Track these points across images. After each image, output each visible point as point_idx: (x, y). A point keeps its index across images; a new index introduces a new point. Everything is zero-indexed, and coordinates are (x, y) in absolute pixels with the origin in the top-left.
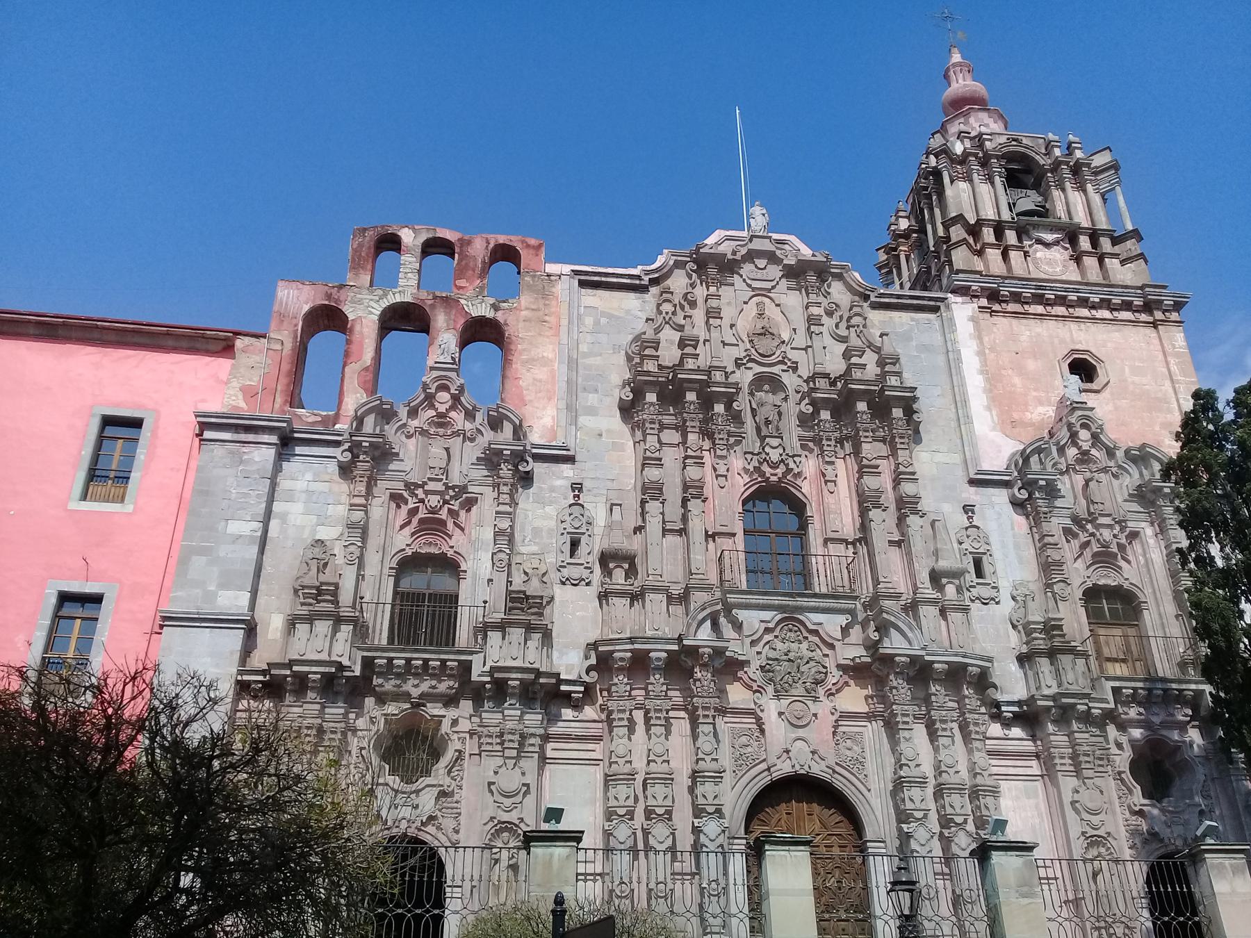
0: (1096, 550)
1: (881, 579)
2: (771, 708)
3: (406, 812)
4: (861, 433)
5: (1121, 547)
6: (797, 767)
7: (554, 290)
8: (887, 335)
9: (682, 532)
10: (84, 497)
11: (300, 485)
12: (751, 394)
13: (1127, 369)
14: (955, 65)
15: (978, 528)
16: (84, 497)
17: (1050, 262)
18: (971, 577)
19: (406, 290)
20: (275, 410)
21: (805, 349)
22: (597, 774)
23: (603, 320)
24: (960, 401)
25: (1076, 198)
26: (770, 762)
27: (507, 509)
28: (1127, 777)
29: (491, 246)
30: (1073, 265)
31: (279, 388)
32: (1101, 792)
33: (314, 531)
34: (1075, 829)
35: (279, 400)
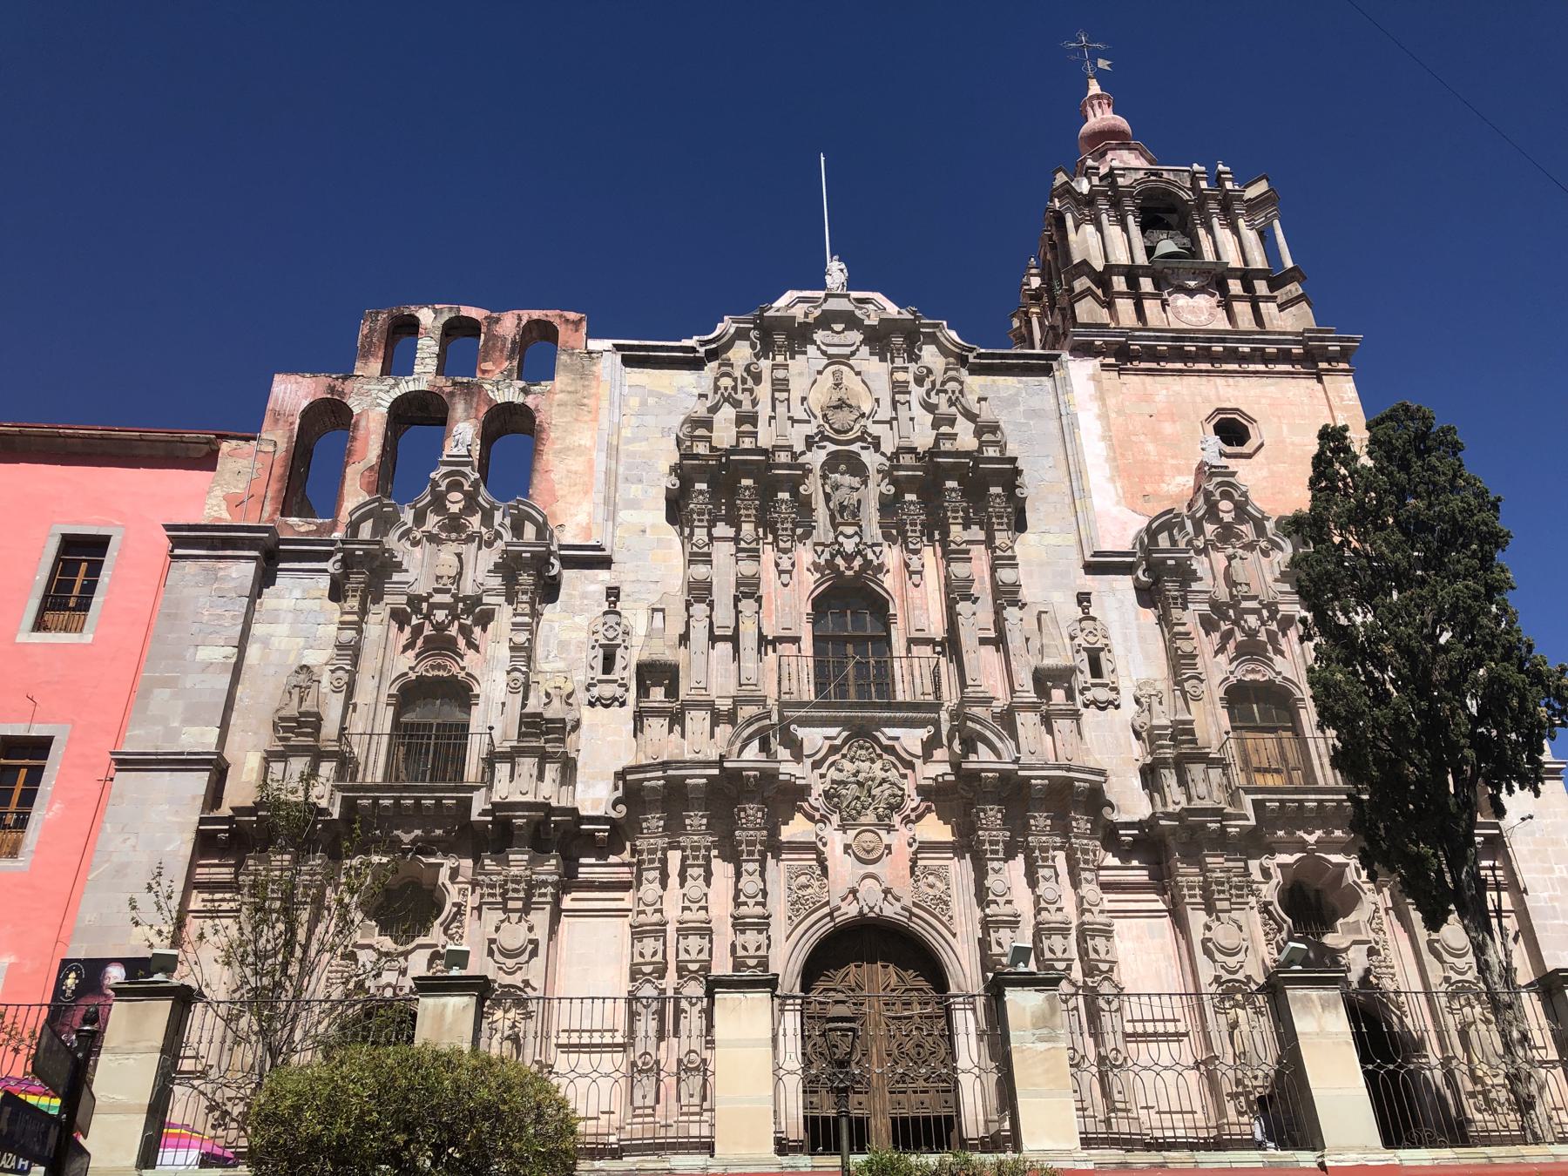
1: (969, 682)
2: (835, 841)
3: (389, 977)
4: (949, 514)
5: (1272, 637)
7: (594, 368)
8: (985, 399)
9: (734, 639)
10: (40, 625)
11: (287, 603)
12: (824, 477)
13: (1285, 428)
14: (1092, 97)
15: (1094, 619)
16: (40, 625)
17: (1193, 311)
18: (1085, 677)
19: (424, 375)
20: (263, 519)
21: (889, 422)
22: (622, 927)
23: (651, 401)
24: (1074, 472)
25: (1224, 235)
27: (527, 619)
28: (1277, 908)
29: (524, 322)
30: (1221, 314)
31: (269, 495)
32: (1240, 928)
33: (301, 655)
34: (1207, 971)
35: (268, 509)
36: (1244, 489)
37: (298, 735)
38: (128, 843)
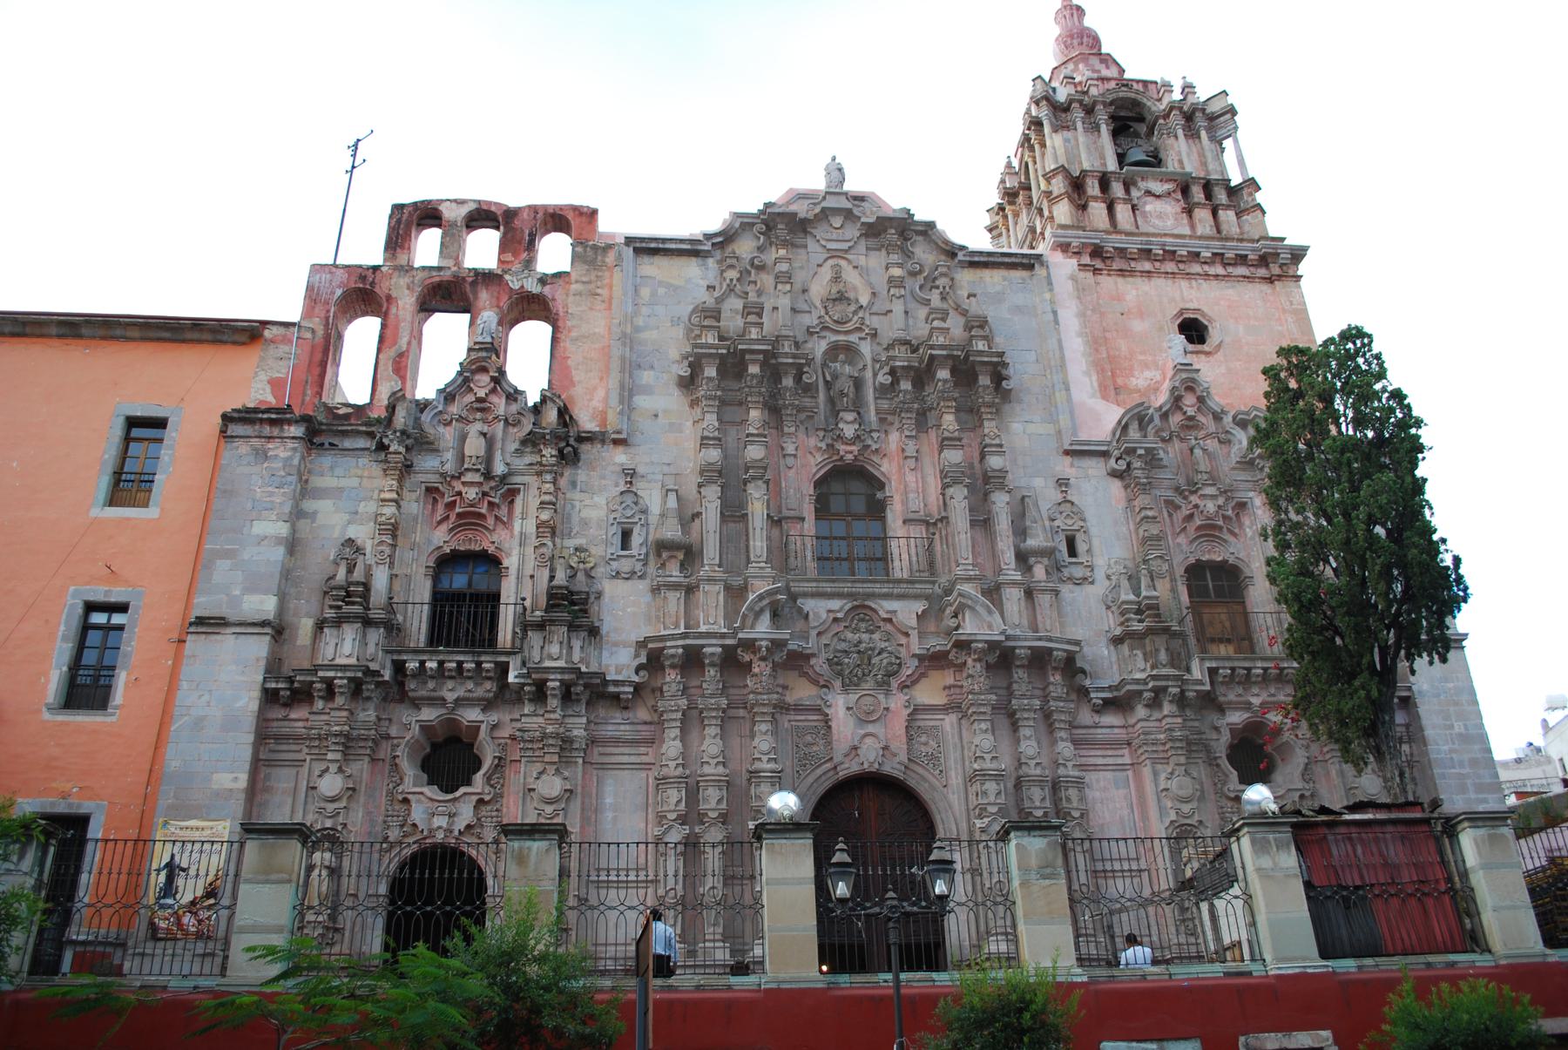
0: (1199, 523)
6: (866, 766)
8: (975, 296)
15: (1073, 503)
17: (1160, 216)
23: (661, 291)
26: (836, 760)
36: (1206, 385)
37: (348, 604)
38: (203, 699)
